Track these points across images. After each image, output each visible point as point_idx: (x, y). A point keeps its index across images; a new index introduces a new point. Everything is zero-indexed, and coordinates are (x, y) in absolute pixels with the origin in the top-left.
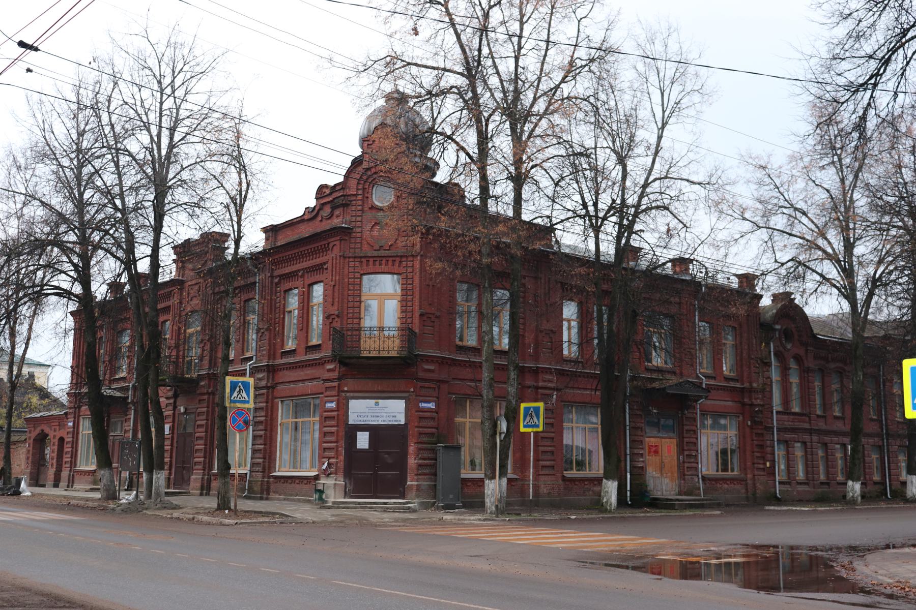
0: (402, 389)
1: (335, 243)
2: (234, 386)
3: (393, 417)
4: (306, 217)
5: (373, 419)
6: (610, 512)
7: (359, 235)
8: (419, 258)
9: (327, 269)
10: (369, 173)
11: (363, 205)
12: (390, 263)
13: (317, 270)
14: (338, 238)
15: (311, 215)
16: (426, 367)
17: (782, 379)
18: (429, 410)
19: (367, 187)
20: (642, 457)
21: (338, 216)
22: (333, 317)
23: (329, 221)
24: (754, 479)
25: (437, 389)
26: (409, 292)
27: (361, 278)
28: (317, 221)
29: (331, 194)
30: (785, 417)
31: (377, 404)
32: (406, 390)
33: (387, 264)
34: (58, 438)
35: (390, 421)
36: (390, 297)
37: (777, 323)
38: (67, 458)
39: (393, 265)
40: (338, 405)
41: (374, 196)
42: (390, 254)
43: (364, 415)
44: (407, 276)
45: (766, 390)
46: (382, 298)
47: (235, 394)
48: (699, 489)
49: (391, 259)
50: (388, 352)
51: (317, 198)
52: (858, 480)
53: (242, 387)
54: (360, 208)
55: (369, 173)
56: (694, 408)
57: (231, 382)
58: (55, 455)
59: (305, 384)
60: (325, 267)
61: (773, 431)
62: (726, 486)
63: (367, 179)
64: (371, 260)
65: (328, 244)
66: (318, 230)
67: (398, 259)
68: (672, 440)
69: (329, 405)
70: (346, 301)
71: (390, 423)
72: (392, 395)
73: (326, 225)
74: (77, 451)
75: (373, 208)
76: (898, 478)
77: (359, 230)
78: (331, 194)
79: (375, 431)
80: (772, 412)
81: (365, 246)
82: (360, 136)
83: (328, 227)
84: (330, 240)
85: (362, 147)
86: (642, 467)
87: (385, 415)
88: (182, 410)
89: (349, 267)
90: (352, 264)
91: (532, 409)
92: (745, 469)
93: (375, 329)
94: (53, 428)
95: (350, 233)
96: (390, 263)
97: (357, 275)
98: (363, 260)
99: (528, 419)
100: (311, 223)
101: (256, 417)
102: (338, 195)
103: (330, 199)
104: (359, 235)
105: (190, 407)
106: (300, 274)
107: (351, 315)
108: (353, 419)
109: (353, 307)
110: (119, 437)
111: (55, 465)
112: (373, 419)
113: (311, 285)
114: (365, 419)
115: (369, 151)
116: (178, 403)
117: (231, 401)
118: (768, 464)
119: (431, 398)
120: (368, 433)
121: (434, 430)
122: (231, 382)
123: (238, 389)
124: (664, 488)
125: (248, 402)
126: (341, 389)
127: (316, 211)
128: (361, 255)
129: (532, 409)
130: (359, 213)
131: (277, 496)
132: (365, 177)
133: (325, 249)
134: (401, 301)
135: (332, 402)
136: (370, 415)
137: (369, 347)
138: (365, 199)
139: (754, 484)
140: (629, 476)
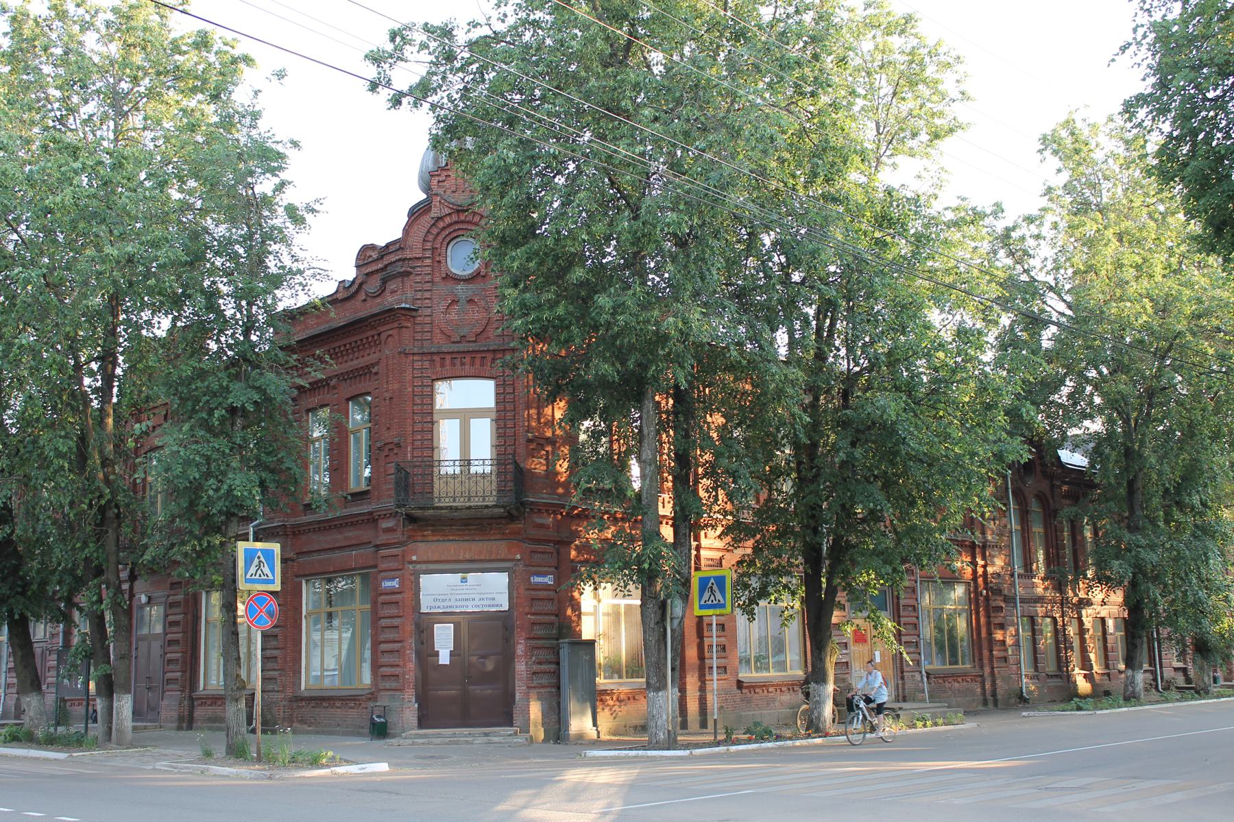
0: (503, 556)
1: (390, 332)
2: (250, 556)
4: (340, 296)
5: (459, 603)
7: (428, 320)
9: (376, 373)
10: (441, 224)
11: (432, 274)
12: (478, 362)
13: (319, 387)
15: (347, 294)
16: (539, 521)
18: (546, 587)
19: (438, 246)
21: (393, 292)
22: (390, 446)
23: (378, 300)
25: (555, 554)
26: (509, 407)
27: (432, 386)
28: (357, 303)
29: (381, 258)
31: (464, 580)
32: (510, 557)
33: (472, 364)
35: (486, 606)
36: (480, 413)
39: (482, 365)
40: (401, 583)
41: (449, 260)
42: (477, 349)
43: (444, 597)
44: (504, 381)
46: (465, 416)
47: (253, 570)
48: (923, 691)
51: (357, 266)
53: (262, 559)
54: (428, 278)
55: (441, 224)
57: (246, 550)
59: (345, 553)
60: (374, 370)
61: (1016, 603)
62: (956, 685)
63: (438, 234)
64: (448, 357)
65: (379, 334)
66: (362, 314)
71: (486, 609)
72: (431, 567)
73: (374, 307)
75: (450, 278)
77: (428, 312)
78: (381, 258)
82: (421, 171)
83: (376, 310)
84: (382, 329)
85: (427, 188)
87: (477, 597)
88: (144, 599)
89: (414, 369)
90: (418, 365)
91: (712, 581)
96: (478, 362)
99: (706, 595)
100: (348, 305)
102: (393, 260)
103: (380, 266)
104: (428, 320)
105: (155, 595)
106: (333, 383)
109: (422, 431)
110: (41, 644)
112: (459, 603)
114: (446, 604)
115: (441, 191)
116: (136, 590)
119: (546, 569)
121: (553, 618)
122: (246, 550)
123: (256, 561)
125: (272, 582)
126: (407, 559)
127: (356, 286)
129: (712, 581)
130: (427, 287)
131: (305, 727)
132: (435, 231)
133: (375, 343)
134: (497, 420)
135: (393, 579)
137: (444, 496)
138: (436, 264)
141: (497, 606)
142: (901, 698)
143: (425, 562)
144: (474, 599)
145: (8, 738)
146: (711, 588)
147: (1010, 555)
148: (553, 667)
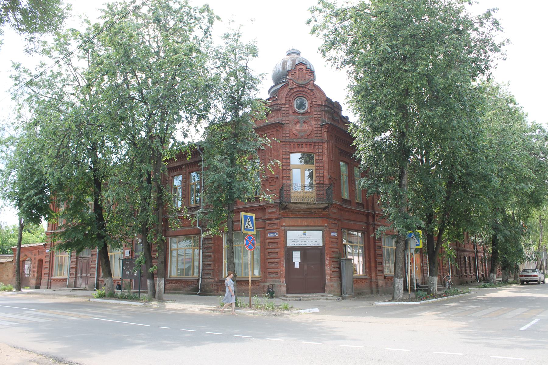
0: (320, 224)
5: (302, 243)
8: (326, 144)
10: (292, 91)
12: (308, 146)
14: (275, 130)
31: (305, 234)
34: (37, 259)
38: (45, 271)
43: (297, 240)
47: (247, 225)
49: (308, 144)
50: (302, 199)
55: (292, 91)
58: (36, 269)
63: (291, 95)
67: (313, 144)
69: (332, 234)
74: (52, 267)
79: (305, 251)
81: (292, 136)
82: (274, 74)
93: (299, 185)
94: (34, 254)
95: (282, 127)
96: (308, 146)
98: (291, 144)
101: (205, 244)
104: (288, 128)
107: (285, 178)
108: (290, 243)
111: (36, 275)
113: (190, 173)
114: (297, 243)
115: (292, 78)
117: (245, 229)
125: (253, 230)
128: (290, 141)
136: (300, 241)
144: (309, 242)
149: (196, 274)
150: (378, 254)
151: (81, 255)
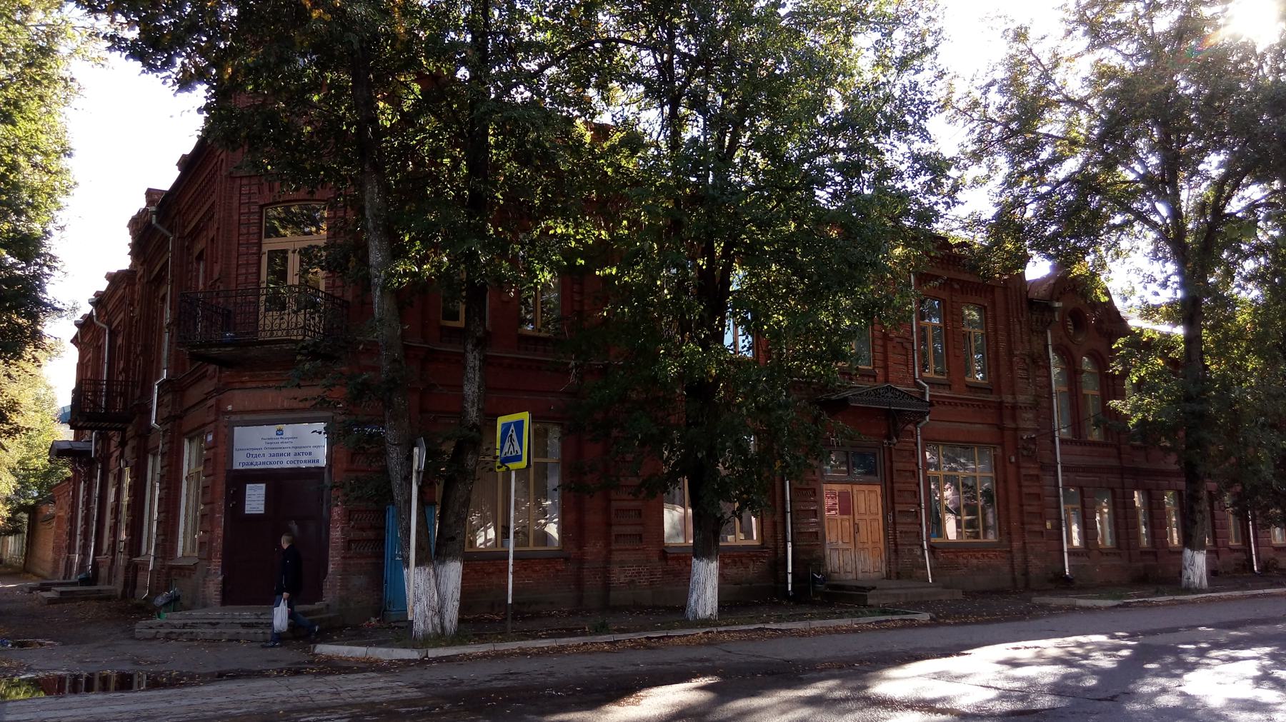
3: (306, 454)
6: (1199, 590)
17: (1070, 390)
20: (816, 517)
24: (1024, 549)
30: (1078, 449)
31: (280, 432)
37: (1058, 300)
45: (1041, 406)
52: (1201, 547)
56: (912, 434)
62: (975, 561)
68: (871, 488)
70: (234, 254)
72: (247, 417)
76: (1270, 542)
79: (277, 481)
80: (1054, 442)
86: (816, 533)
91: (512, 428)
92: (1009, 534)
97: (255, 208)
118: (1049, 525)
120: (263, 485)
124: (860, 567)
129: (512, 428)
136: (267, 452)
139: (1025, 560)
140: (790, 550)
141: (314, 461)
142: (893, 575)
143: (242, 412)
144: (289, 455)
145: (1136, 697)
146: (511, 435)
147: (111, 429)
148: (370, 534)
149: (1052, 473)
150: (1025, 475)
151: (959, 231)
